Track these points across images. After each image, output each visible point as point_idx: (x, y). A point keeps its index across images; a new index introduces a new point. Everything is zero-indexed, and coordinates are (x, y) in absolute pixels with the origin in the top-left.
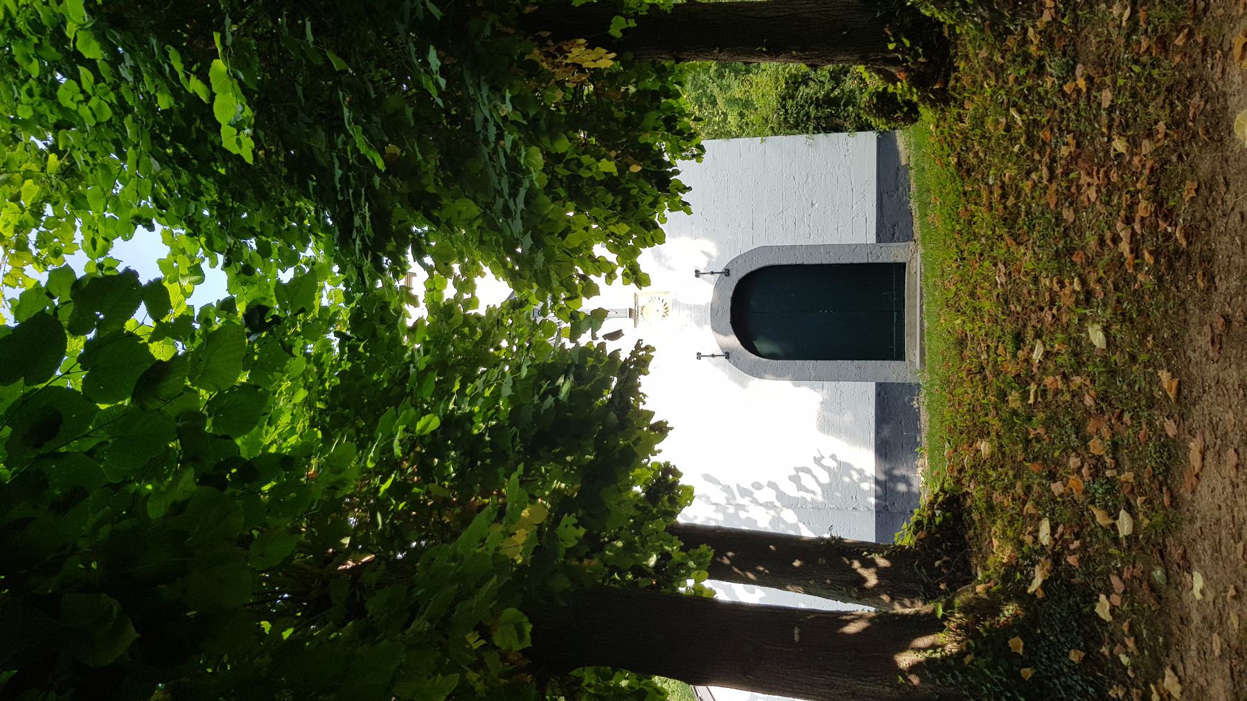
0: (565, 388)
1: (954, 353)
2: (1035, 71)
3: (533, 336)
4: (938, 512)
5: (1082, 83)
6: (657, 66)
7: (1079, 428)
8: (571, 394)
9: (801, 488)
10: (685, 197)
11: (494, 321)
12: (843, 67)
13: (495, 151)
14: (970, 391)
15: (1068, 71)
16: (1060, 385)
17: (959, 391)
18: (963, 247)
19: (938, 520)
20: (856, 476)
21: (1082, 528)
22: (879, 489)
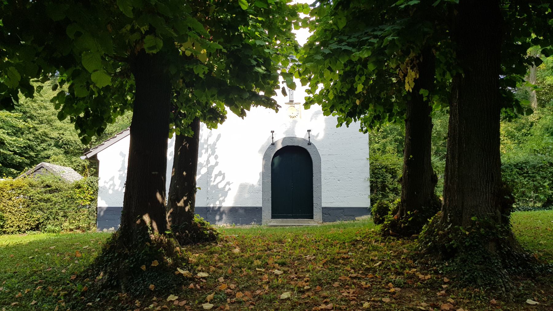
0: (260, 70)
1: (276, 238)
2: (397, 271)
3: (282, 56)
4: (209, 232)
5: (392, 290)
6: (404, 112)
7: (247, 288)
8: (257, 73)
9: (216, 176)
10: (344, 124)
11: (290, 38)
12: (399, 193)
13: (369, 35)
14: (260, 245)
15: (397, 285)
16: (264, 281)
17: (260, 241)
18: (321, 242)
19: (205, 232)
20: (221, 199)
21: (205, 289)
22: (217, 208)
